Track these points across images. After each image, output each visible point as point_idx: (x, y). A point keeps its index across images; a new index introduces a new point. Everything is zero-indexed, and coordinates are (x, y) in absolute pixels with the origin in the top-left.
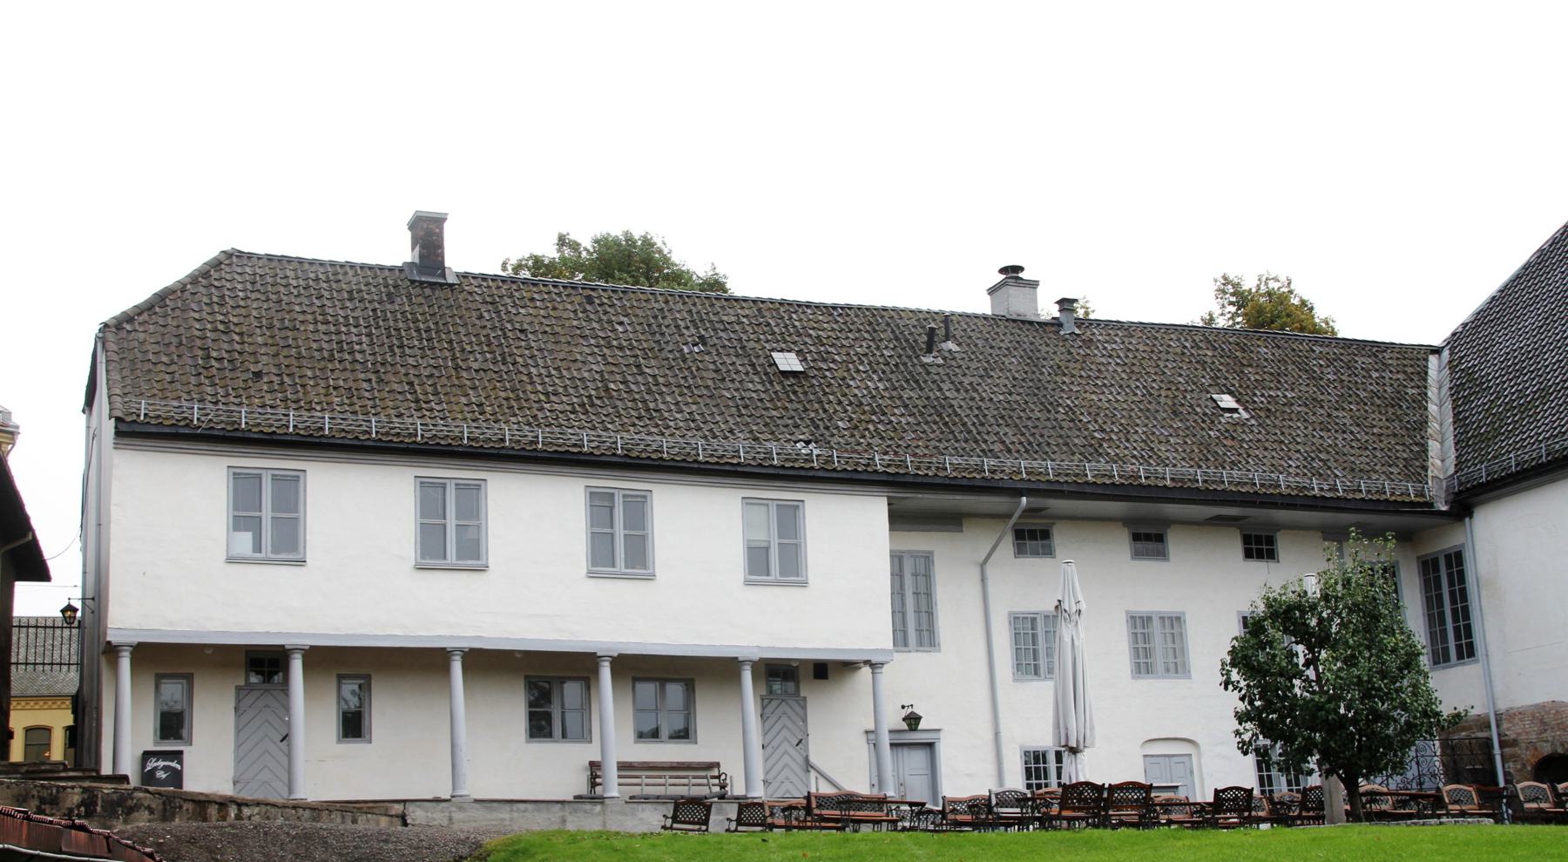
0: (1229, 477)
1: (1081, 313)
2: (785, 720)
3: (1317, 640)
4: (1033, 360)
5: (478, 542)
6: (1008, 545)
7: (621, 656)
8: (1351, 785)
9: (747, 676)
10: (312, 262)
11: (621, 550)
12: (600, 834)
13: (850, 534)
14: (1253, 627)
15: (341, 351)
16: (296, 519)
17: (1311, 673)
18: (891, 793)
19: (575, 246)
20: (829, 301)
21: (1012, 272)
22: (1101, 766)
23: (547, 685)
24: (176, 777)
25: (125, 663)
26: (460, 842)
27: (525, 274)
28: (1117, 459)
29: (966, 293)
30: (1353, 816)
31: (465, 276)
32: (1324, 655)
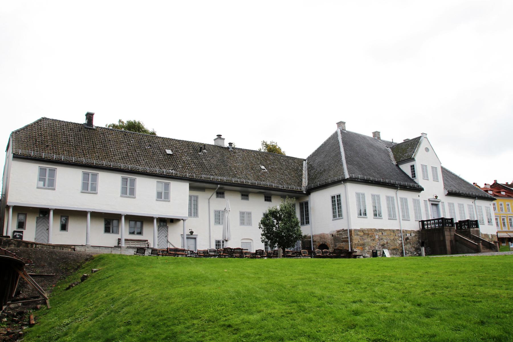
0: (262, 183)
1: (233, 146)
3: (279, 219)
4: (222, 155)
6: (215, 195)
7: (127, 215)
8: (284, 250)
9: (155, 221)
10: (62, 121)
11: (129, 191)
12: (120, 255)
13: (180, 190)
14: (266, 216)
17: (277, 226)
18: (186, 248)
19: (123, 122)
20: (179, 139)
22: (232, 244)
23: (110, 221)
24: (21, 237)
26: (87, 255)
27: (111, 128)
28: (239, 178)
29: (210, 140)
30: (284, 256)
31: (97, 127)
32: (280, 222)
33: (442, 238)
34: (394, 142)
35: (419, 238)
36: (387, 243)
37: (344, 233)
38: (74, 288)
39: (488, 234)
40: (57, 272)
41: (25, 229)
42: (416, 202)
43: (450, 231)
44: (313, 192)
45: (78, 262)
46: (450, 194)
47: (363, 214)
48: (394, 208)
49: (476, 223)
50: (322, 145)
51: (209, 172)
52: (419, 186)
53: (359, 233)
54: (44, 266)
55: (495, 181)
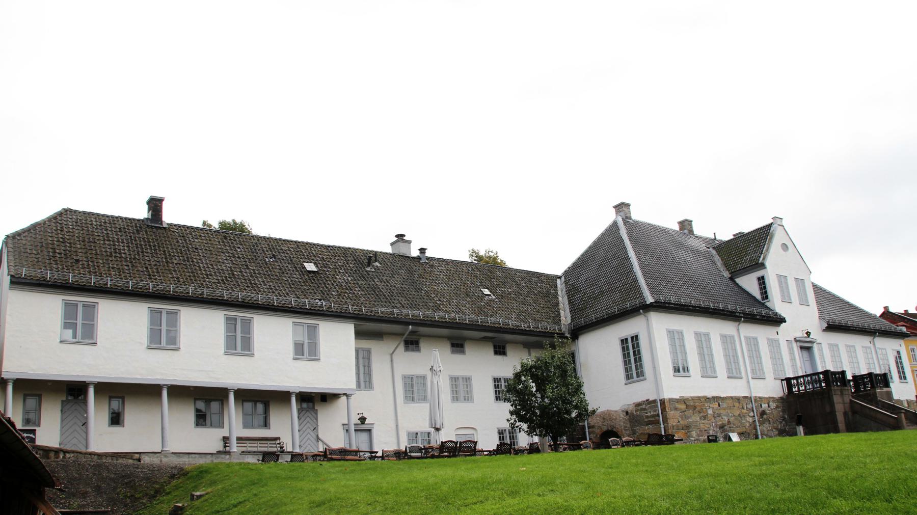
0: (491, 320)
2: (308, 419)
4: (410, 272)
5: (175, 338)
6: (402, 347)
9: (294, 399)
10: (103, 216)
13: (338, 339)
15: (115, 252)
16: (93, 325)
20: (327, 244)
21: (400, 237)
23: (205, 401)
26: (175, 468)
28: (446, 311)
31: (171, 225)
33: (828, 409)
34: (718, 238)
35: (783, 411)
36: (729, 422)
37: (651, 407)
39: (902, 399)
40: (115, 504)
41: (39, 425)
42: (774, 344)
43: (842, 394)
44: (582, 334)
45: (157, 483)
46: (832, 328)
47: (680, 370)
48: (735, 356)
49: (884, 380)
50: (590, 247)
51: (389, 301)
52: (776, 314)
53: (678, 406)
54: (86, 492)
55: (886, 308)
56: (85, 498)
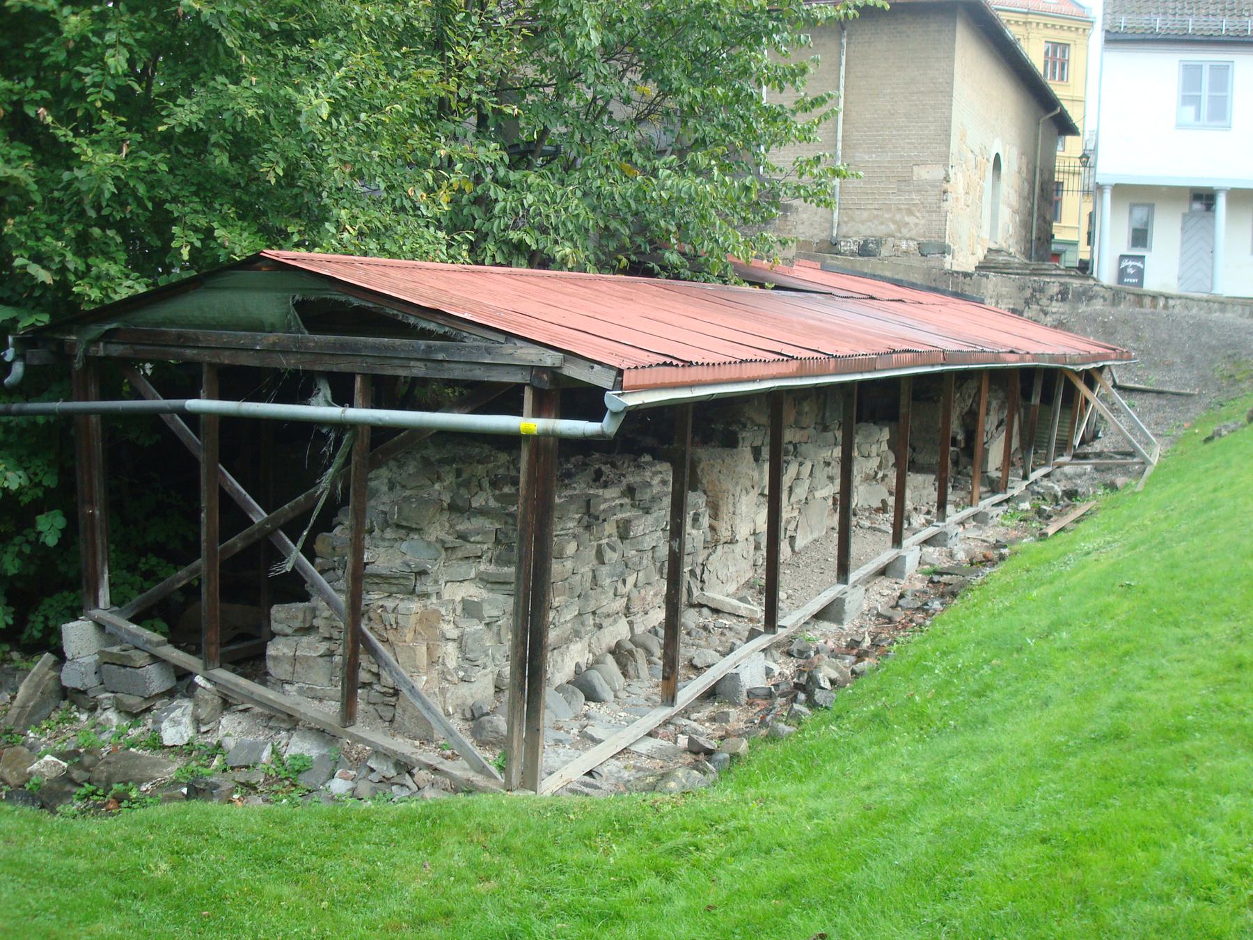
24: (1140, 273)
25: (1107, 196)
38: (1223, 440)
40: (1206, 385)
41: (1150, 250)
54: (1173, 364)
56: (1169, 371)
